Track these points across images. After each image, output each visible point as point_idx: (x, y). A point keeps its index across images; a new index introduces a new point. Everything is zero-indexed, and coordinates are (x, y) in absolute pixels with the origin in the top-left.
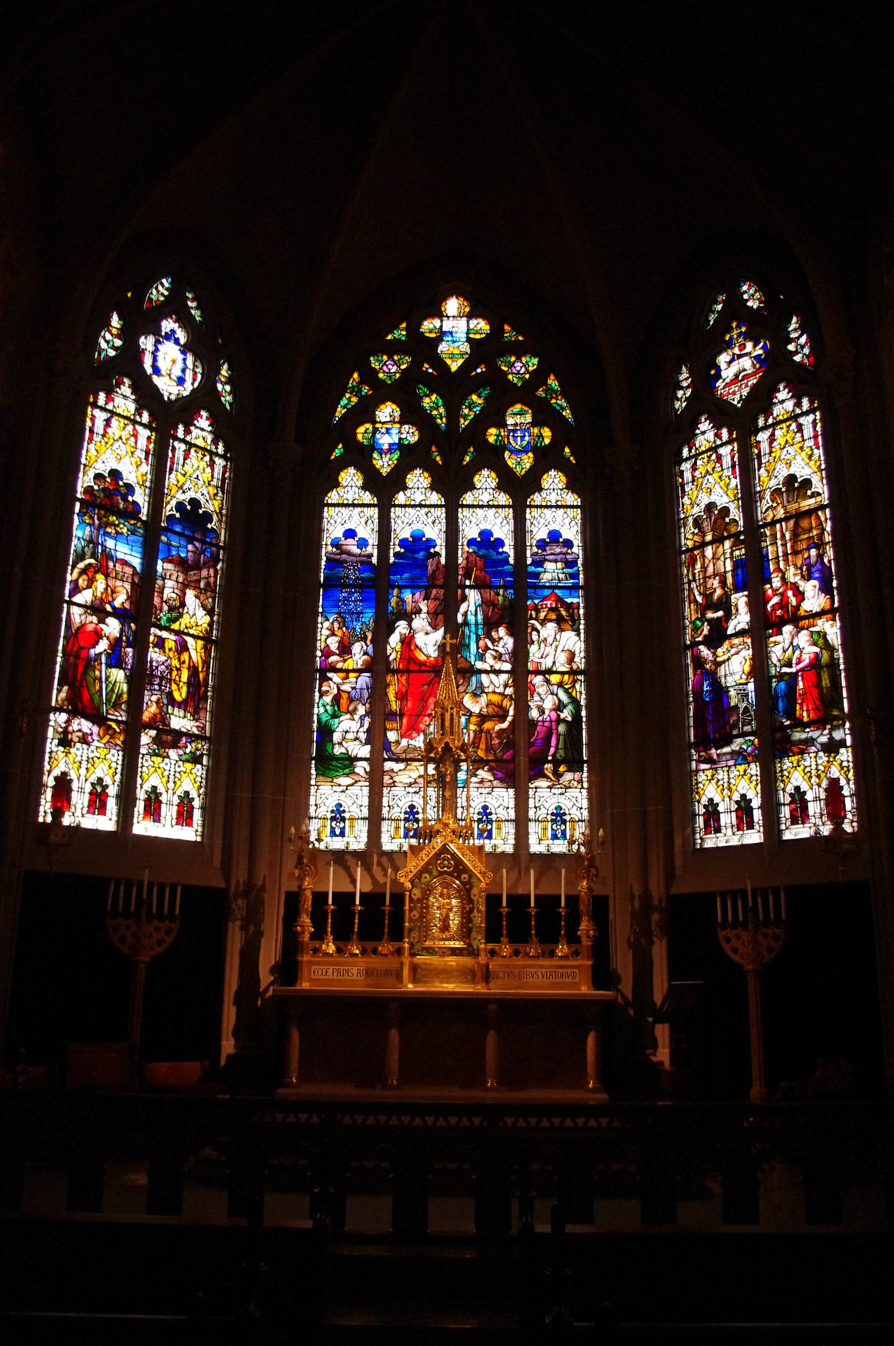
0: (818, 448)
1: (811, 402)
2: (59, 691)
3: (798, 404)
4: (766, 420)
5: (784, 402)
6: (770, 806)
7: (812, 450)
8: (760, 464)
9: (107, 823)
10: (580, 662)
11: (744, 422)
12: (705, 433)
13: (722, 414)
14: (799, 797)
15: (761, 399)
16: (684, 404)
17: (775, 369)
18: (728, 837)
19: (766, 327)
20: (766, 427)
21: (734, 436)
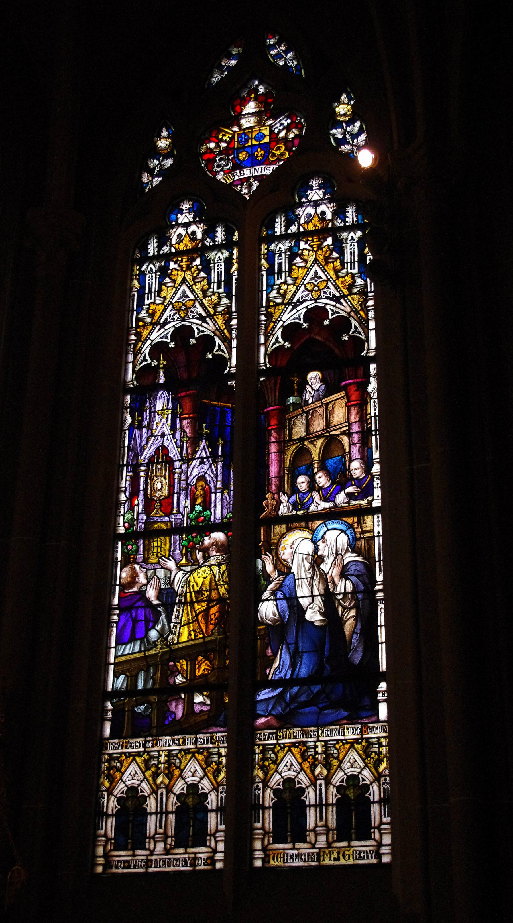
0: (229, 296)
1: (229, 234)
2: (342, 305)
3: (340, 213)
4: (287, 227)
5: (316, 205)
6: (240, 807)
7: (220, 298)
8: (141, 303)
9: (214, 852)
10: (381, 534)
11: (248, 222)
12: (186, 227)
13: (218, 206)
14: (290, 799)
15: (282, 193)
16: (157, 180)
17: (315, 158)
18: (159, 854)
19: (302, 98)
20: (158, 258)
21: (235, 238)
